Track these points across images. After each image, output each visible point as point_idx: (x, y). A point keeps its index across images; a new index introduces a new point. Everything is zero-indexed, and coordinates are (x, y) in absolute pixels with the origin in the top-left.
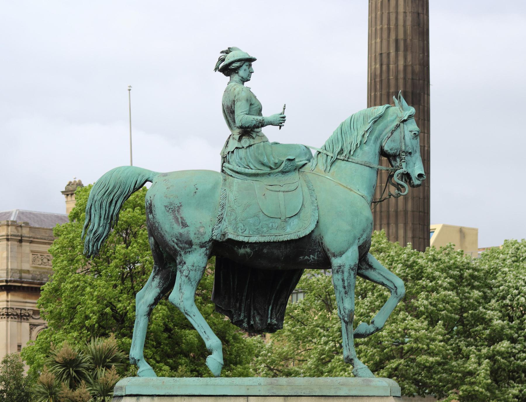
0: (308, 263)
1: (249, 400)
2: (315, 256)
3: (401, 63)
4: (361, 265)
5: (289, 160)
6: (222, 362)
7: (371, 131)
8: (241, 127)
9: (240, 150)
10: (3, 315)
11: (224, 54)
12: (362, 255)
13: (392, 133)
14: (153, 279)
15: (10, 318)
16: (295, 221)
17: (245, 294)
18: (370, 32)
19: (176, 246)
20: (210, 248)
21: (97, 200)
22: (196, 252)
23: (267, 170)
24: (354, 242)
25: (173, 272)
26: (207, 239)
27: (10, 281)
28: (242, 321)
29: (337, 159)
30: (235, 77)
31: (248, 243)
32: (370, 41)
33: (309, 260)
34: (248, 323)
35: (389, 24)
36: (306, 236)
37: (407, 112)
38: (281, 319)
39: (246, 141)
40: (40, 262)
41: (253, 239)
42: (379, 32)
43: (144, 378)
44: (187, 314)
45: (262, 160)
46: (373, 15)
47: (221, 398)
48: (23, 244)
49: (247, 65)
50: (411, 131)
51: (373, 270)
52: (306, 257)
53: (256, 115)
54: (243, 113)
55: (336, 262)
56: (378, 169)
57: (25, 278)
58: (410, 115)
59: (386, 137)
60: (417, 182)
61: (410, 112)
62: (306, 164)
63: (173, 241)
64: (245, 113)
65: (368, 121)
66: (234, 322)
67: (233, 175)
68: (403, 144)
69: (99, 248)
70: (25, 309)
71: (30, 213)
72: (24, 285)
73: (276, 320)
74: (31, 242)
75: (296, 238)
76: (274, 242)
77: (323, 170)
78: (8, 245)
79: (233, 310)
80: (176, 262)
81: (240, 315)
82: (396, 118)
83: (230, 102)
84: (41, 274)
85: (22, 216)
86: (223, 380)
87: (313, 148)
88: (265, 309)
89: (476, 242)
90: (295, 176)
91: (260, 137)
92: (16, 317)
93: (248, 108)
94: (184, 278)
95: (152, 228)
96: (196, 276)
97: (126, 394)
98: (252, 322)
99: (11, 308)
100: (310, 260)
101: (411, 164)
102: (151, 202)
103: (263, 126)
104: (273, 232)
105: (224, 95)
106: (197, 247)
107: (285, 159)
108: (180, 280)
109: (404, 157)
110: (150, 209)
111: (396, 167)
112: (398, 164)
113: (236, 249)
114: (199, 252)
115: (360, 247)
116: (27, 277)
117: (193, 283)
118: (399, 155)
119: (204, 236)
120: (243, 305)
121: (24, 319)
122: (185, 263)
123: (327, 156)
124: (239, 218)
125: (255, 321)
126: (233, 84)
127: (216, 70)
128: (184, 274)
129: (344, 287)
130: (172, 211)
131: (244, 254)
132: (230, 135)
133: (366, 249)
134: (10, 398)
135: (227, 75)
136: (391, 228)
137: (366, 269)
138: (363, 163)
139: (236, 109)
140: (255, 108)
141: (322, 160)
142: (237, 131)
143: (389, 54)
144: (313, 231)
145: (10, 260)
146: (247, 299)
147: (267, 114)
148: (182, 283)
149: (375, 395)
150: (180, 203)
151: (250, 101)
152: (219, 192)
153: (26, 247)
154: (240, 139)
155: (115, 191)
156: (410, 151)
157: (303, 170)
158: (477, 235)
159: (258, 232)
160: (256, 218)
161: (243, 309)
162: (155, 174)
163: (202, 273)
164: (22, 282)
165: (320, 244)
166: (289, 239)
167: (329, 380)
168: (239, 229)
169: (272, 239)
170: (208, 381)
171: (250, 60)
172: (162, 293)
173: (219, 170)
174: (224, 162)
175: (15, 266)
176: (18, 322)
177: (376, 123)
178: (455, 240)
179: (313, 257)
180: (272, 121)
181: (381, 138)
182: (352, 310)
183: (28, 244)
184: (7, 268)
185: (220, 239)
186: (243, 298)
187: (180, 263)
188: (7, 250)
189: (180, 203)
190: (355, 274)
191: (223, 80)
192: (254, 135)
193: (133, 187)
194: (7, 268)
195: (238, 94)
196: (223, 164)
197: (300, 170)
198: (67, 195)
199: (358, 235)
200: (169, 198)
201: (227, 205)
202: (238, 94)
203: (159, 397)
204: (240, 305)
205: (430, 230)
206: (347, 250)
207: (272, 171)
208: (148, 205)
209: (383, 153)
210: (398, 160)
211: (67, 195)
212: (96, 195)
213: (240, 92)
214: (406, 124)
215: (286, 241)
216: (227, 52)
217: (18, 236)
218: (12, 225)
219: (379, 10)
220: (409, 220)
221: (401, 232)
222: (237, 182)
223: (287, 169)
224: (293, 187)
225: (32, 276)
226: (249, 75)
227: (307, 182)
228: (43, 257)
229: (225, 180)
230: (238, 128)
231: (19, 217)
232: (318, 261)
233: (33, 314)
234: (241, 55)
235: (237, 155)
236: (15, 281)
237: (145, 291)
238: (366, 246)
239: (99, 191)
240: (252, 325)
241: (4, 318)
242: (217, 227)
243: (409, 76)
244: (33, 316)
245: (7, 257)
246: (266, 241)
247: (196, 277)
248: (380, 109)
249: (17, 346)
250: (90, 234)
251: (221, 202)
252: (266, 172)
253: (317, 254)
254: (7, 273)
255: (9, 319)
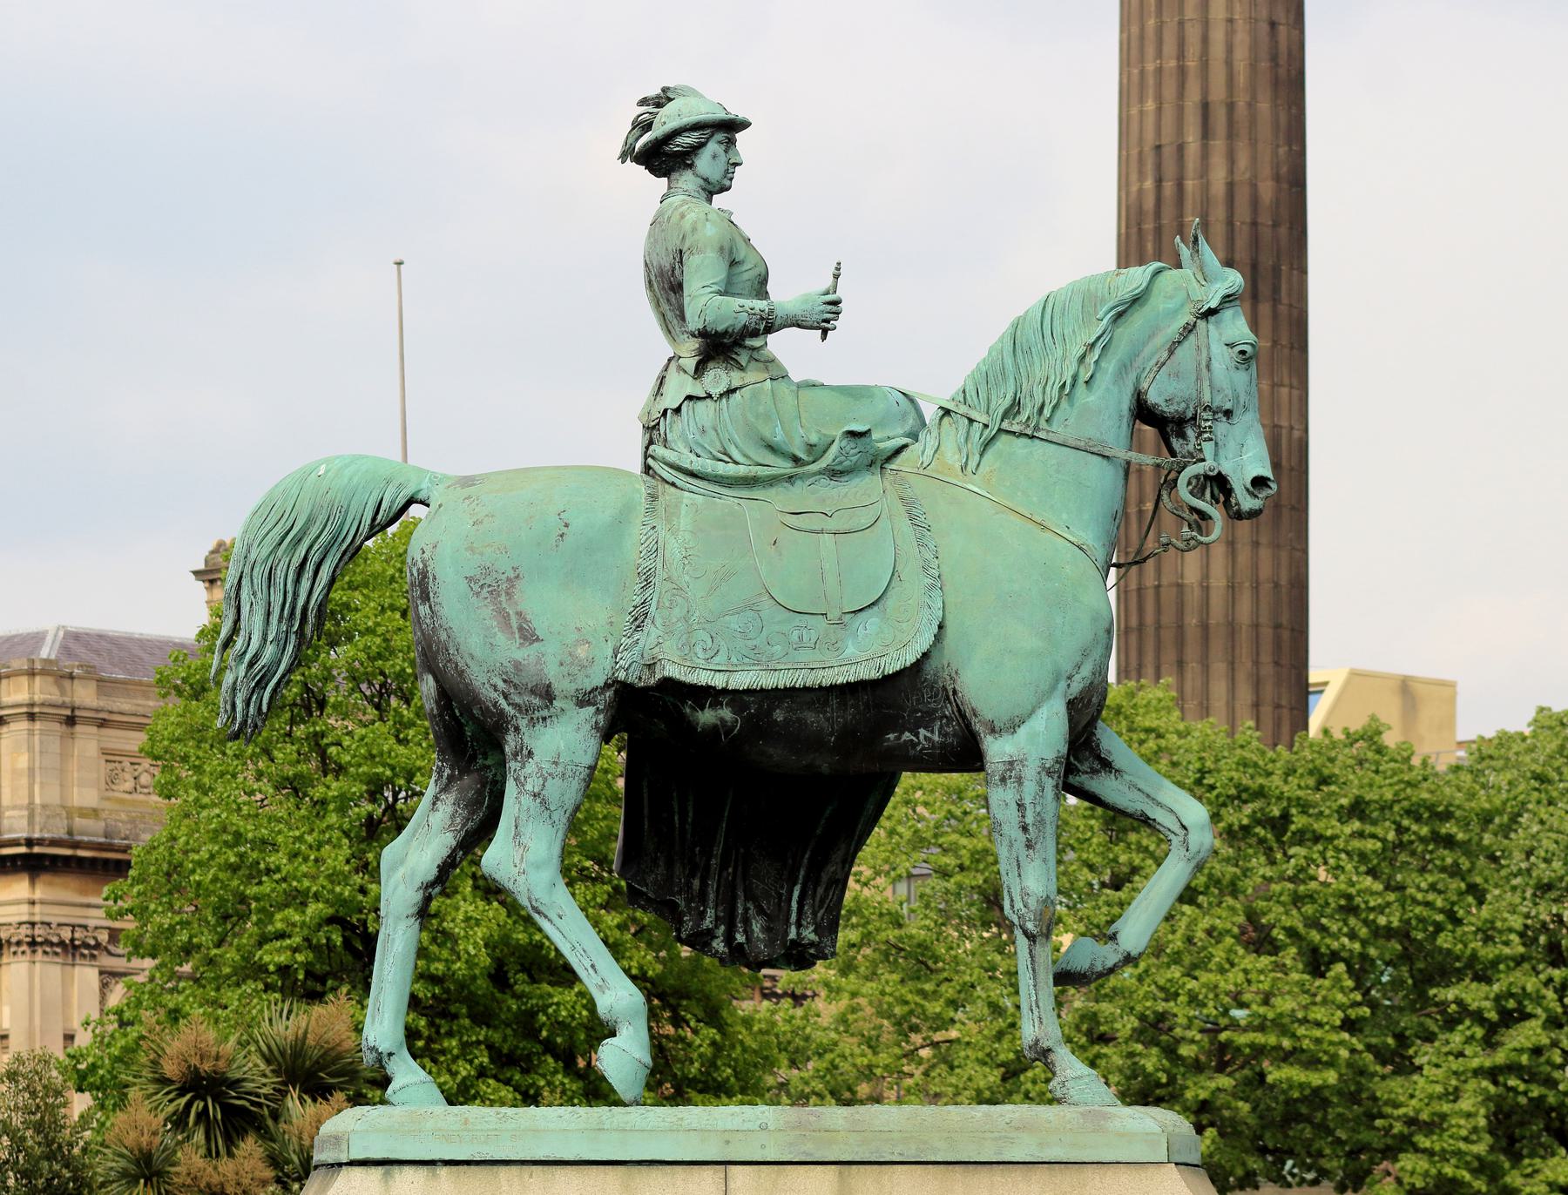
0: (912, 753)
1: (729, 1175)
2: (932, 732)
3: (1219, 176)
4: (1076, 758)
5: (853, 434)
6: (648, 1060)
7: (1101, 345)
8: (703, 334)
9: (700, 405)
10: (19, 943)
11: (651, 109)
12: (1080, 727)
13: (1171, 352)
14: (434, 804)
15: (40, 950)
16: (872, 620)
17: (718, 850)
18: (1125, 81)
19: (502, 702)
20: (609, 707)
21: (259, 560)
22: (563, 719)
23: (785, 467)
24: (1053, 688)
25: (495, 782)
26: (599, 681)
27: (40, 842)
28: (710, 934)
29: (1000, 430)
30: (684, 178)
31: (725, 691)
32: (1125, 110)
33: (913, 745)
34: (729, 938)
35: (1181, 56)
36: (905, 668)
37: (1218, 286)
38: (829, 927)
39: (718, 378)
40: (129, 785)
41: (741, 681)
42: (1151, 81)
43: (405, 1108)
44: (539, 913)
45: (767, 434)
46: (1135, 30)
47: (643, 1168)
48: (78, 728)
49: (720, 142)
50: (1230, 345)
51: (1112, 776)
52: (907, 734)
53: (749, 296)
54: (710, 290)
55: (997, 750)
56: (1128, 463)
57: (81, 834)
58: (1229, 296)
59: (1153, 362)
60: (1247, 503)
61: (1227, 284)
62: (905, 446)
63: (495, 688)
64: (715, 288)
65: (1096, 313)
66: (683, 936)
67: (678, 482)
68: (1206, 384)
69: (265, 708)
70: (85, 927)
71: (101, 637)
72: (82, 853)
73: (815, 931)
74: (103, 724)
75: (874, 675)
76: (806, 689)
77: (958, 466)
78: (31, 732)
79: (680, 901)
80: (503, 752)
81: (702, 915)
82: (1182, 305)
83: (667, 255)
84: (132, 821)
85: (73, 645)
86: (651, 1114)
87: (929, 400)
88: (780, 895)
89: (1449, 722)
90: (867, 485)
91: (761, 365)
92: (58, 950)
93: (723, 275)
94: (527, 800)
95: (430, 647)
96: (566, 792)
97: (352, 1157)
98: (740, 938)
99: (42, 923)
100: (919, 743)
101: (1232, 445)
102: (425, 566)
103: (769, 329)
104: (805, 656)
105: (650, 235)
106: (570, 705)
107: (839, 433)
108: (517, 806)
109: (1209, 423)
110: (423, 586)
111: (1184, 457)
112: (1191, 447)
113: (688, 710)
114: (575, 721)
115: (1071, 704)
116: (90, 830)
117: (555, 816)
118: (1194, 418)
119: (590, 671)
120: (712, 884)
121: (83, 956)
122: (530, 754)
123: (971, 421)
124: (697, 614)
125: (748, 932)
126: (676, 200)
127: (623, 157)
128: (529, 787)
129: (1025, 829)
130: (491, 593)
131: (715, 727)
132: (670, 360)
133: (1092, 710)
134: (26, 1186)
135: (657, 171)
136: (1189, 675)
137: (1094, 772)
138: (1082, 444)
139: (686, 278)
140: (747, 274)
141: (952, 433)
142: (689, 349)
143: (1181, 149)
144: (925, 655)
145: (38, 779)
146: (723, 866)
147: (785, 293)
148: (524, 817)
149: (1120, 1160)
150: (514, 569)
151: (731, 252)
152: (636, 533)
153: (88, 741)
154: (700, 370)
155: (314, 531)
156: (1228, 406)
157: (893, 467)
158: (1452, 701)
159: (756, 658)
160: (751, 614)
161: (712, 896)
162: (436, 480)
163: (583, 784)
164: (76, 845)
165: (949, 695)
166: (852, 679)
167: (979, 1115)
168: (698, 649)
169: (800, 679)
170: (604, 1118)
171: (731, 127)
172: (461, 849)
173: (636, 467)
174: (651, 442)
175: (54, 797)
176: (63, 964)
177: (1123, 319)
178: (1390, 713)
179: (929, 735)
180: (800, 313)
181: (1136, 365)
182: (1048, 897)
183: (94, 729)
184: (31, 803)
185: (640, 678)
186: (713, 861)
187: (515, 755)
188: (31, 749)
189: (514, 569)
190: (1057, 786)
191: (646, 185)
192: (743, 359)
193: (369, 522)
194: (31, 803)
195: (694, 230)
196: (647, 448)
197: (886, 466)
198: (212, 582)
199: (1067, 667)
200: (482, 554)
201: (661, 574)
202: (694, 230)
203: (454, 1168)
204: (704, 885)
205: (1307, 685)
206: (1033, 712)
207: (800, 470)
208: (416, 574)
209: (1143, 412)
210: (1190, 433)
211: (212, 582)
212: (255, 545)
213: (699, 226)
214: (1217, 323)
215: (842, 685)
216: (662, 99)
217: (63, 706)
218: (43, 672)
219: (1153, 15)
220: (1244, 651)
221: (1219, 689)
222: (690, 501)
223: (847, 463)
224: (865, 521)
225: (107, 826)
226: (727, 171)
227: (910, 506)
228: (140, 769)
229: (653, 497)
230: (694, 335)
231: (66, 650)
232: (943, 746)
233: (109, 942)
234: (703, 110)
235: (691, 421)
236: (54, 843)
237: (408, 842)
238: (1090, 700)
239: (264, 532)
240: (741, 945)
241: (23, 953)
242: (629, 641)
243: (1243, 213)
244: (111, 948)
245: (31, 770)
246: (781, 686)
247: (566, 798)
248: (1138, 276)
249: (61, 1038)
250: (237, 666)
251: (639, 565)
252: (782, 471)
253: (941, 727)
254: (31, 817)
255: (39, 955)
